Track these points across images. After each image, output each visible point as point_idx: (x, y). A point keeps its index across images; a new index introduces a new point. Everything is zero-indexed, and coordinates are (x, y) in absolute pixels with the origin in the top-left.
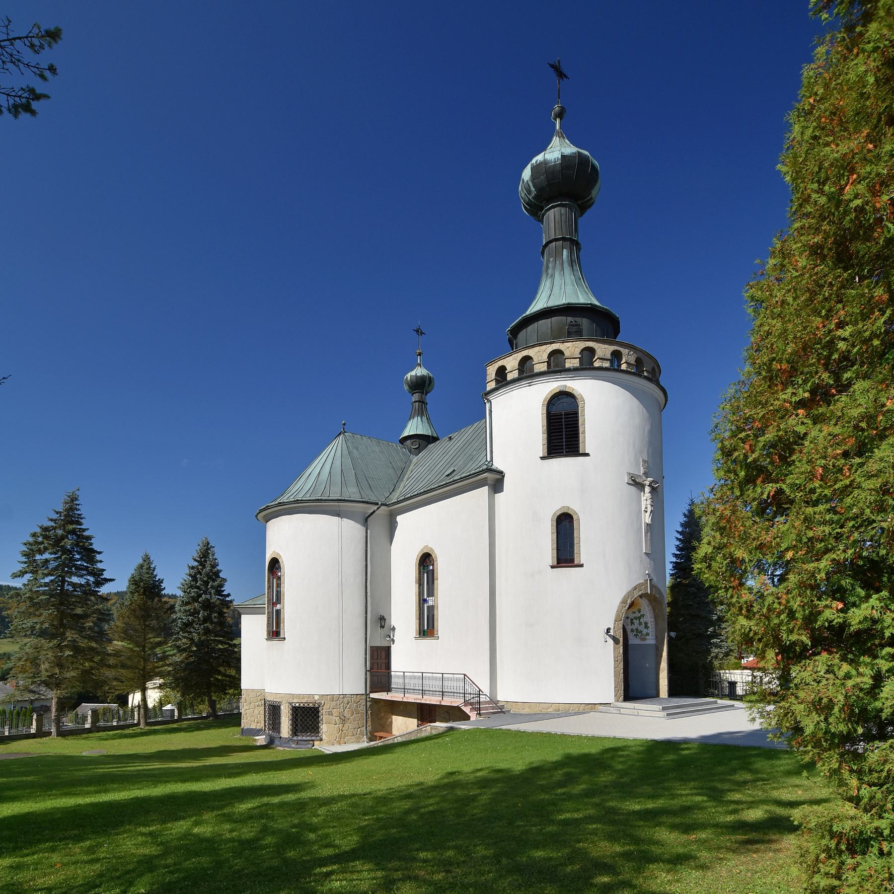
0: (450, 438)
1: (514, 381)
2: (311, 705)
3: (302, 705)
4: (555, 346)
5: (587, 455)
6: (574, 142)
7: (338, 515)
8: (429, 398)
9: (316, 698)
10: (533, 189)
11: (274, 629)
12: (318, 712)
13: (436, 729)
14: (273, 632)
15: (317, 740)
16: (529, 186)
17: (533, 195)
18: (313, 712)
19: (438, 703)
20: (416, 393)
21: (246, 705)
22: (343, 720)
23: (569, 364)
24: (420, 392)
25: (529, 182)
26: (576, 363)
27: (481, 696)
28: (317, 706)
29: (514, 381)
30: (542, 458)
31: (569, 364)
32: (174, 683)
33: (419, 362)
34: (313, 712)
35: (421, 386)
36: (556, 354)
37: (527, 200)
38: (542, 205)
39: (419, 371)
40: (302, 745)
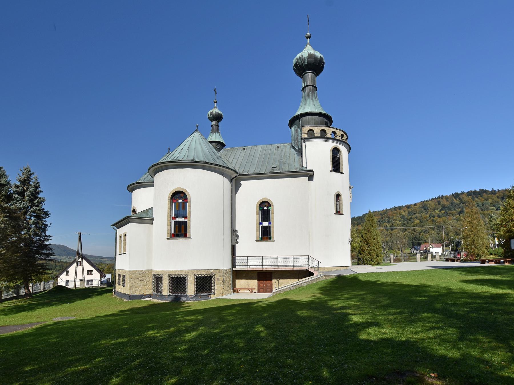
0: (244, 149)
1: (317, 138)
2: (209, 275)
3: (203, 275)
4: (323, 128)
5: (343, 173)
6: (320, 53)
7: (222, 175)
8: (220, 124)
9: (212, 271)
10: (306, 62)
11: (173, 233)
12: (186, 280)
13: (328, 277)
14: (172, 234)
15: (212, 294)
16: (305, 60)
17: (305, 64)
18: (183, 280)
19: (292, 269)
20: (216, 121)
21: (132, 281)
22: (224, 282)
23: (316, 135)
24: (217, 121)
25: (306, 59)
26: (319, 135)
27: (294, 266)
28: (184, 276)
29: (317, 138)
30: (331, 171)
31: (316, 135)
32: (503, 254)
33: (215, 106)
34: (183, 280)
35: (218, 118)
36: (323, 131)
37: (301, 64)
38: (306, 69)
39: (215, 111)
40: (204, 298)
